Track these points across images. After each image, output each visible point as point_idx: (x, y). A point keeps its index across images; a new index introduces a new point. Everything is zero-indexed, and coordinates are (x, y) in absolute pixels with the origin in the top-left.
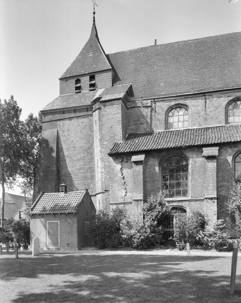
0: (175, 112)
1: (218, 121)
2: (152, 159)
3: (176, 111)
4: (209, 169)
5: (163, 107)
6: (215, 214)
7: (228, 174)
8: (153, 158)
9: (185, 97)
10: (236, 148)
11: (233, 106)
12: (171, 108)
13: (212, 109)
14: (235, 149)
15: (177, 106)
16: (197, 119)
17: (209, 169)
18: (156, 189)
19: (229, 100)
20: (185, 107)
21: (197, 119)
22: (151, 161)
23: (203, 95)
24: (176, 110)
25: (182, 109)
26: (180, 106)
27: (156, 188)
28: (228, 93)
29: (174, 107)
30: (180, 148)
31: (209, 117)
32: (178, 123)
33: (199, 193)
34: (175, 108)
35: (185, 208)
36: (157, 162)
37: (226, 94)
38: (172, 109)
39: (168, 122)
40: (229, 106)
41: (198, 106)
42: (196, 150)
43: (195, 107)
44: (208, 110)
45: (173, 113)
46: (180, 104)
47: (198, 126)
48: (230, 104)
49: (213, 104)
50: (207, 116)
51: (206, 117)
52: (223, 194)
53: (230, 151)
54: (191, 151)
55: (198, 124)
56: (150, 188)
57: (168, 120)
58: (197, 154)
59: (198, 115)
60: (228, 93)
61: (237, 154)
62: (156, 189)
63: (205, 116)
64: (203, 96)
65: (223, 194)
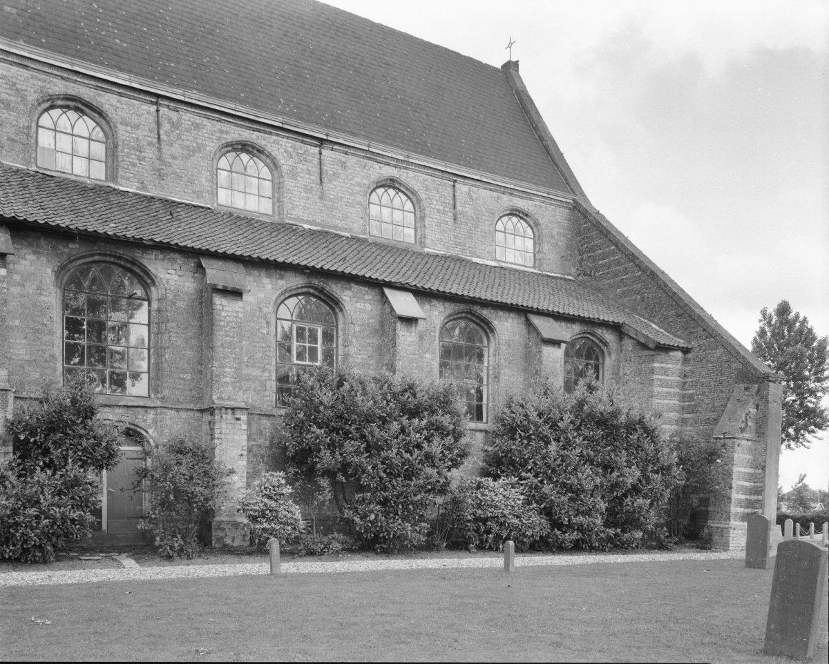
0: (65, 119)
1: (194, 192)
2: (31, 257)
3: (64, 115)
4: (222, 323)
5: (24, 88)
6: (241, 455)
7: (262, 347)
8: (34, 253)
9: (99, 85)
10: (284, 282)
11: (231, 162)
12: (52, 103)
13: (176, 149)
14: (280, 282)
15: (70, 103)
16: (134, 165)
17: (222, 323)
18: (46, 361)
19: (223, 142)
20: (94, 114)
21: (134, 165)
22: (27, 263)
23: (154, 100)
24: (64, 112)
25: (85, 117)
26: (80, 105)
27: (47, 356)
28: (220, 121)
29: (60, 103)
30: (137, 244)
31: (170, 170)
32: (238, 158)
33: (184, 390)
34: (61, 107)
35: (143, 432)
36: (49, 271)
37: (215, 122)
38: (52, 107)
39: (37, 142)
40: (220, 158)
41: (137, 127)
42: (179, 261)
43: (129, 128)
44: (165, 148)
45: (55, 120)
46: (80, 100)
47: (138, 188)
48: (224, 155)
49: (179, 137)
50: (164, 167)
51: (161, 169)
52: (250, 401)
53: (269, 287)
54: (163, 260)
55: (138, 182)
56: (23, 351)
57: (37, 137)
58: (180, 273)
59: (138, 153)
60: (220, 121)
61: (283, 298)
62: (46, 361)
63: (158, 164)
64: (152, 103)
65: (250, 401)
